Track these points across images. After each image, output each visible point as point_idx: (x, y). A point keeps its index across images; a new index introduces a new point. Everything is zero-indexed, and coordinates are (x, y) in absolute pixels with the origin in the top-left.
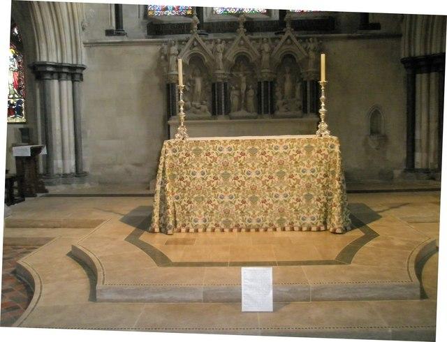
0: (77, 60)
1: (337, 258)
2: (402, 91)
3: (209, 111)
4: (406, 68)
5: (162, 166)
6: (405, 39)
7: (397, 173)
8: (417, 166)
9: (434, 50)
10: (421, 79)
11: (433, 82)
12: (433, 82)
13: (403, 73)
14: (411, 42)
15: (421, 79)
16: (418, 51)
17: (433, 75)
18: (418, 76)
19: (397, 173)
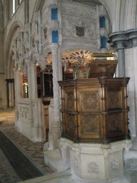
0: (10, 77)
1: (56, 44)
2: (6, 88)
3: (128, 70)
4: (6, 81)
5: (21, 81)
6: (5, 74)
7: (5, 108)
8: (10, 106)
9: (12, 78)
10: (10, 84)
11: (12, 85)
12: (12, 85)
13: (6, 82)
14: (7, 75)
15: (10, 84)
16: (8, 78)
17: (12, 83)
18: (9, 83)
19: (5, 108)
